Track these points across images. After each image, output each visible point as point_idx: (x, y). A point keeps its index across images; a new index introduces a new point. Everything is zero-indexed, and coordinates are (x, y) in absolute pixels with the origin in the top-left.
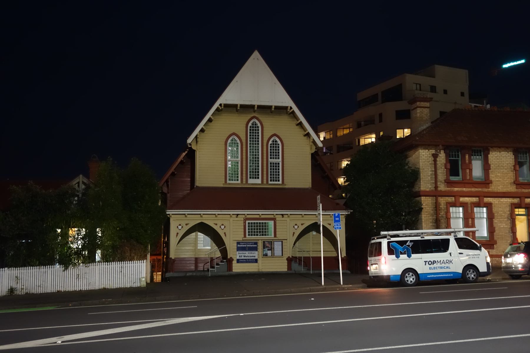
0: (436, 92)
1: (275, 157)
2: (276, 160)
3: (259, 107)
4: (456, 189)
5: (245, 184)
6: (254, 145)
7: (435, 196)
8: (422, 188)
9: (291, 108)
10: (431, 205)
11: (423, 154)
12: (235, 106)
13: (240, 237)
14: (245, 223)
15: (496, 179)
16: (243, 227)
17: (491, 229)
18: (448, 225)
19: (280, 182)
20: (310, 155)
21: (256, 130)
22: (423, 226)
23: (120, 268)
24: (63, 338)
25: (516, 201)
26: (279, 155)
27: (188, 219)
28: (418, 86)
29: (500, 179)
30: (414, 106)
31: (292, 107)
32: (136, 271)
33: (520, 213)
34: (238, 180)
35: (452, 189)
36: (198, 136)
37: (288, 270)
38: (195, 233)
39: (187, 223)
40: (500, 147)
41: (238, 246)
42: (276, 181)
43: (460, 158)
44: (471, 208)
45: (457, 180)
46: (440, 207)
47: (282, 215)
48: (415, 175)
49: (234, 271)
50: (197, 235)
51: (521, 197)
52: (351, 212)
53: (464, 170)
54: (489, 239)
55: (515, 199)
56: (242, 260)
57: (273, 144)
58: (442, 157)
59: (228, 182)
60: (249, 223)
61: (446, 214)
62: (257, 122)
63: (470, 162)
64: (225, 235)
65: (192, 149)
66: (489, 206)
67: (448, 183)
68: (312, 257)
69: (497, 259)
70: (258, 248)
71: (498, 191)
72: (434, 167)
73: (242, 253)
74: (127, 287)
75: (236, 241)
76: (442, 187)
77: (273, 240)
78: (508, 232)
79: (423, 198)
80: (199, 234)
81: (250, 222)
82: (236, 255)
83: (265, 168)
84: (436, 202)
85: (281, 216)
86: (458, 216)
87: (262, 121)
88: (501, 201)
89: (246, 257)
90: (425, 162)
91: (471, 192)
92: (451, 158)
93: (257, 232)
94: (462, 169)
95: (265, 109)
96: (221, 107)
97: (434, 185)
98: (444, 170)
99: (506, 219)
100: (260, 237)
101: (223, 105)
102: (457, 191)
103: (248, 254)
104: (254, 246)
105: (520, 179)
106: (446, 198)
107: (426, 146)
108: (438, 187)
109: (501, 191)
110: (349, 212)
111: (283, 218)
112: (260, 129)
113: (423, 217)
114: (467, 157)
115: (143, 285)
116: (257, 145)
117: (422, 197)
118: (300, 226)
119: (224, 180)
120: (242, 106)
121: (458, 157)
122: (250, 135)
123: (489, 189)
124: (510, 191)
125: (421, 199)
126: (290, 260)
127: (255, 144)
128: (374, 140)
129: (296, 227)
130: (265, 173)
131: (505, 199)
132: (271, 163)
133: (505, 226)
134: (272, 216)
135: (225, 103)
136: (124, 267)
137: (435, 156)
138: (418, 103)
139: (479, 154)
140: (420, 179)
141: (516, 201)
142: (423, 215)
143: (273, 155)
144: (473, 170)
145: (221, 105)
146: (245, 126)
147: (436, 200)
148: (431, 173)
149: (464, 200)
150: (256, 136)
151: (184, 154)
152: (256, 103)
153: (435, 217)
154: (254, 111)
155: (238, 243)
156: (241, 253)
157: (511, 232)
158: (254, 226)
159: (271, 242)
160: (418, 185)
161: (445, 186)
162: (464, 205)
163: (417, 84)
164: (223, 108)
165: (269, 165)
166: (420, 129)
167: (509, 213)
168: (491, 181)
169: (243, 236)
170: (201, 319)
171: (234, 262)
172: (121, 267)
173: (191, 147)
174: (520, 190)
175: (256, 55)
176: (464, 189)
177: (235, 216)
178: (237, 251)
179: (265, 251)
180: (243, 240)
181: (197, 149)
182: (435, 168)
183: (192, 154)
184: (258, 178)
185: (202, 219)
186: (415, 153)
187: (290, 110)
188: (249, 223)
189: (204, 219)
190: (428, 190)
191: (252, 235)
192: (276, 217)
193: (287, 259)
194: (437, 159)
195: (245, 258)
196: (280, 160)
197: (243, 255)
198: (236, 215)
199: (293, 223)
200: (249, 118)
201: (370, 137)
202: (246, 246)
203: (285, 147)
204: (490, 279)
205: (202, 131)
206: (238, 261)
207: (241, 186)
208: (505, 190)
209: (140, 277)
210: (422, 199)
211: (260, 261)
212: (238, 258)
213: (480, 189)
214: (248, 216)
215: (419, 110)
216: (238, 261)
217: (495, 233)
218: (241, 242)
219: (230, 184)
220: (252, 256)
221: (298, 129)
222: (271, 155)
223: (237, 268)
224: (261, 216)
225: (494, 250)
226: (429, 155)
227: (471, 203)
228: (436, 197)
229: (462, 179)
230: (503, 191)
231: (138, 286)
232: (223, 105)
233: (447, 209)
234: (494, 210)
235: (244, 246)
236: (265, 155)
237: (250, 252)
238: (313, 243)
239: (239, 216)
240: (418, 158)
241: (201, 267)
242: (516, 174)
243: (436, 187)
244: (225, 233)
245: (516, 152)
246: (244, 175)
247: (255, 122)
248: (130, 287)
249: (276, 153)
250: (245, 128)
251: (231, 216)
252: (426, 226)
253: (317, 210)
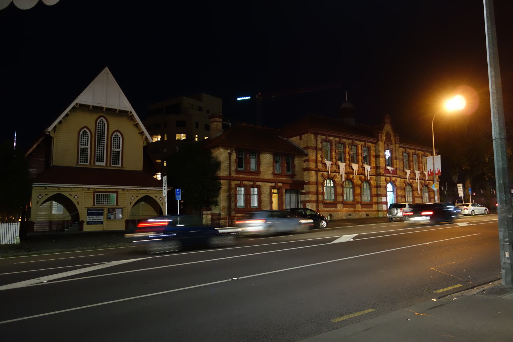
0: (202, 111)
1: (116, 147)
2: (85, 146)
4: (241, 176)
7: (229, 180)
9: (131, 112)
13: (90, 205)
14: (94, 194)
15: (264, 171)
17: (259, 201)
18: (235, 198)
19: (120, 166)
25: (273, 184)
27: (47, 190)
29: (265, 171)
30: (212, 120)
31: (132, 112)
32: (11, 231)
33: (275, 192)
35: (239, 175)
38: (50, 202)
39: (138, 195)
40: (267, 151)
41: (88, 211)
42: (117, 164)
46: (232, 187)
47: (123, 190)
48: (218, 165)
49: (84, 230)
50: (52, 204)
51: (276, 182)
52: (172, 189)
54: (244, 208)
56: (91, 223)
57: (116, 137)
61: (235, 192)
62: (104, 120)
63: (250, 160)
64: (78, 204)
66: (259, 187)
67: (237, 172)
72: (229, 161)
73: (92, 217)
75: (87, 209)
76: (233, 174)
77: (115, 207)
78: (268, 203)
79: (222, 181)
80: (54, 202)
81: (98, 194)
85: (122, 190)
86: (241, 193)
90: (224, 158)
91: (249, 178)
94: (245, 163)
95: (111, 112)
97: (228, 173)
98: (235, 164)
100: (101, 205)
101: (78, 105)
103: (96, 218)
104: (101, 212)
105: (276, 171)
106: (235, 181)
107: (225, 147)
108: (231, 174)
109: (266, 178)
114: (248, 156)
117: (221, 180)
118: (135, 197)
121: (243, 156)
123: (259, 177)
124: (270, 179)
127: (102, 136)
128: (159, 139)
129: (133, 198)
131: (267, 183)
132: (113, 151)
134: (115, 190)
135: (80, 103)
137: (230, 154)
139: (254, 155)
140: (221, 168)
141: (273, 184)
143: (115, 146)
144: (251, 164)
145: (77, 104)
146: (94, 122)
148: (227, 165)
151: (41, 140)
152: (105, 106)
153: (228, 193)
154: (103, 112)
155: (88, 210)
157: (270, 203)
158: (101, 197)
161: (235, 174)
162: (244, 186)
164: (78, 106)
165: (112, 152)
167: (269, 192)
168: (261, 172)
169: (92, 204)
171: (85, 224)
175: (107, 70)
176: (246, 176)
178: (87, 215)
179: (109, 215)
180: (92, 207)
181: (54, 136)
183: (49, 140)
184: (103, 162)
185: (59, 191)
186: (217, 151)
189: (62, 191)
190: (225, 176)
191: (99, 204)
192: (118, 191)
193: (125, 221)
194: (231, 156)
195: (93, 221)
196: (121, 149)
200: (98, 116)
201: (157, 137)
202: (94, 211)
203: (124, 141)
205: (60, 122)
206: (88, 223)
207: (89, 167)
208: (267, 178)
210: (221, 182)
211: (105, 223)
212: (88, 220)
213: (254, 177)
214: (97, 190)
216: (88, 223)
218: (91, 209)
219: (81, 165)
220: (99, 219)
221: (134, 129)
222: (113, 145)
223: (87, 228)
226: (226, 153)
229: (281, 172)
232: (78, 105)
234: (262, 190)
235: (93, 212)
237: (97, 216)
241: (54, 229)
243: (230, 174)
244: (78, 202)
245: (275, 155)
247: (102, 120)
248: (5, 244)
250: (94, 124)
252: (222, 199)
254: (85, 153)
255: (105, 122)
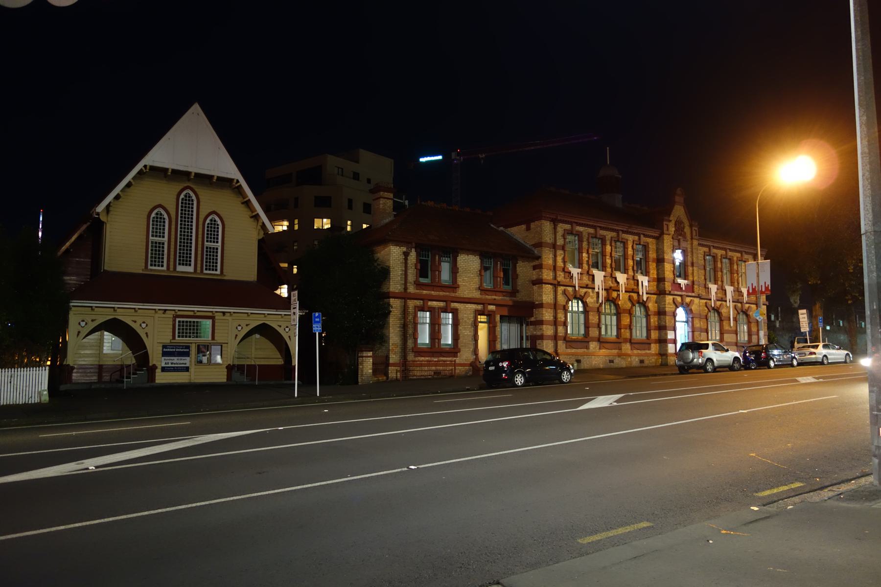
2: (214, 244)
3: (197, 175)
4: (425, 292)
5: (172, 272)
6: (187, 223)
8: (391, 289)
9: (238, 181)
10: (399, 308)
11: (394, 251)
12: (164, 171)
13: (167, 339)
14: (174, 321)
15: (464, 284)
16: (171, 327)
19: (218, 272)
20: (257, 242)
21: (189, 204)
22: (391, 331)
23: (9, 378)
24: (83, 463)
26: (217, 239)
28: (340, 170)
29: (467, 284)
31: (240, 181)
33: (482, 320)
34: (162, 266)
35: (421, 291)
36: (111, 204)
37: (227, 379)
38: (100, 332)
39: (94, 318)
41: (164, 350)
42: (213, 270)
43: (430, 259)
44: (438, 313)
45: (426, 282)
47: (224, 313)
48: (385, 273)
49: (157, 381)
50: (102, 336)
52: (306, 313)
53: (433, 271)
55: (479, 305)
56: (168, 369)
57: (211, 224)
58: (413, 255)
59: (150, 267)
60: (179, 322)
61: (414, 319)
62: (192, 194)
64: (147, 336)
65: (100, 220)
66: (455, 312)
67: (418, 285)
68: (258, 365)
69: (460, 368)
70: (190, 353)
71: (465, 296)
73: (169, 360)
74: (19, 404)
76: (412, 289)
77: (210, 343)
78: (471, 339)
79: (392, 301)
80: (106, 333)
81: (181, 320)
82: (161, 361)
83: (199, 252)
84: (404, 305)
85: (221, 314)
87: (199, 193)
88: (467, 306)
89: (175, 364)
91: (439, 296)
92: (421, 258)
93: (190, 333)
94: (431, 271)
95: (204, 179)
96: (146, 169)
99: (470, 326)
100: (193, 339)
101: (148, 167)
102: (426, 295)
103: (176, 361)
104: (185, 350)
105: (485, 284)
106: (415, 301)
107: (398, 243)
110: (304, 312)
111: (224, 316)
112: (195, 203)
113: (391, 321)
114: (437, 257)
115: (45, 400)
116: (190, 224)
117: (391, 299)
118: (244, 326)
119: (144, 264)
120: (175, 172)
121: (428, 257)
122: (182, 210)
123: (456, 294)
125: (390, 300)
126: (230, 368)
127: (188, 222)
128: (285, 228)
129: (239, 328)
130: (199, 258)
131: (470, 305)
132: (207, 248)
133: (469, 334)
134: (210, 314)
135: (151, 164)
136: (16, 375)
137: (406, 255)
138: (382, 193)
140: (390, 279)
141: (480, 307)
142: (391, 319)
143: (211, 238)
145: (145, 166)
146: (175, 197)
147: (405, 303)
148: (401, 272)
149: (432, 304)
150: (189, 211)
151: (84, 227)
152: (194, 170)
154: (189, 180)
155: (164, 347)
156: (167, 360)
159: (208, 346)
160: (386, 286)
162: (431, 310)
163: (339, 168)
164: (147, 170)
165: (205, 249)
166: (382, 222)
167: (473, 319)
168: (459, 285)
169: (171, 338)
170: (238, 435)
171: (158, 371)
172: (10, 375)
173: (99, 218)
174: (484, 297)
175: (196, 108)
177: (161, 312)
178: (163, 356)
180: (171, 343)
181: (107, 221)
182: (405, 268)
183: (98, 227)
184: (190, 265)
187: (236, 184)
188: (179, 322)
189: (120, 314)
190: (397, 291)
191: (183, 337)
192: (215, 315)
193: (227, 367)
195: (173, 365)
196: (220, 244)
197: (170, 361)
198: (163, 311)
199: (236, 324)
201: (281, 224)
202: (174, 350)
204: (469, 388)
205: (117, 197)
206: (164, 369)
208: (470, 296)
209: (40, 389)
211: (192, 370)
212: (163, 365)
213: (448, 293)
215: (382, 201)
216: (164, 369)
217: (459, 341)
218: (168, 345)
219: (151, 270)
220: (182, 364)
221: (243, 209)
222: (207, 238)
223: (161, 378)
224: (214, 314)
225: (458, 358)
227: (438, 308)
228: (405, 299)
230: (469, 297)
231: (36, 402)
232: (148, 167)
233: (415, 314)
234: (460, 316)
235: (171, 350)
236: (200, 236)
237: (179, 358)
238: (256, 349)
239: (167, 312)
240: (389, 254)
242: (481, 279)
243: (406, 289)
244: (146, 333)
246: (172, 260)
247: (189, 194)
248: (23, 403)
249: (214, 235)
251: (156, 312)
252: (393, 331)
253: (290, 309)
254: (159, 251)
255: (194, 198)
